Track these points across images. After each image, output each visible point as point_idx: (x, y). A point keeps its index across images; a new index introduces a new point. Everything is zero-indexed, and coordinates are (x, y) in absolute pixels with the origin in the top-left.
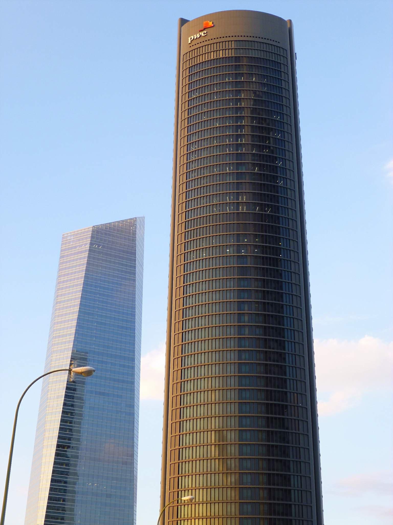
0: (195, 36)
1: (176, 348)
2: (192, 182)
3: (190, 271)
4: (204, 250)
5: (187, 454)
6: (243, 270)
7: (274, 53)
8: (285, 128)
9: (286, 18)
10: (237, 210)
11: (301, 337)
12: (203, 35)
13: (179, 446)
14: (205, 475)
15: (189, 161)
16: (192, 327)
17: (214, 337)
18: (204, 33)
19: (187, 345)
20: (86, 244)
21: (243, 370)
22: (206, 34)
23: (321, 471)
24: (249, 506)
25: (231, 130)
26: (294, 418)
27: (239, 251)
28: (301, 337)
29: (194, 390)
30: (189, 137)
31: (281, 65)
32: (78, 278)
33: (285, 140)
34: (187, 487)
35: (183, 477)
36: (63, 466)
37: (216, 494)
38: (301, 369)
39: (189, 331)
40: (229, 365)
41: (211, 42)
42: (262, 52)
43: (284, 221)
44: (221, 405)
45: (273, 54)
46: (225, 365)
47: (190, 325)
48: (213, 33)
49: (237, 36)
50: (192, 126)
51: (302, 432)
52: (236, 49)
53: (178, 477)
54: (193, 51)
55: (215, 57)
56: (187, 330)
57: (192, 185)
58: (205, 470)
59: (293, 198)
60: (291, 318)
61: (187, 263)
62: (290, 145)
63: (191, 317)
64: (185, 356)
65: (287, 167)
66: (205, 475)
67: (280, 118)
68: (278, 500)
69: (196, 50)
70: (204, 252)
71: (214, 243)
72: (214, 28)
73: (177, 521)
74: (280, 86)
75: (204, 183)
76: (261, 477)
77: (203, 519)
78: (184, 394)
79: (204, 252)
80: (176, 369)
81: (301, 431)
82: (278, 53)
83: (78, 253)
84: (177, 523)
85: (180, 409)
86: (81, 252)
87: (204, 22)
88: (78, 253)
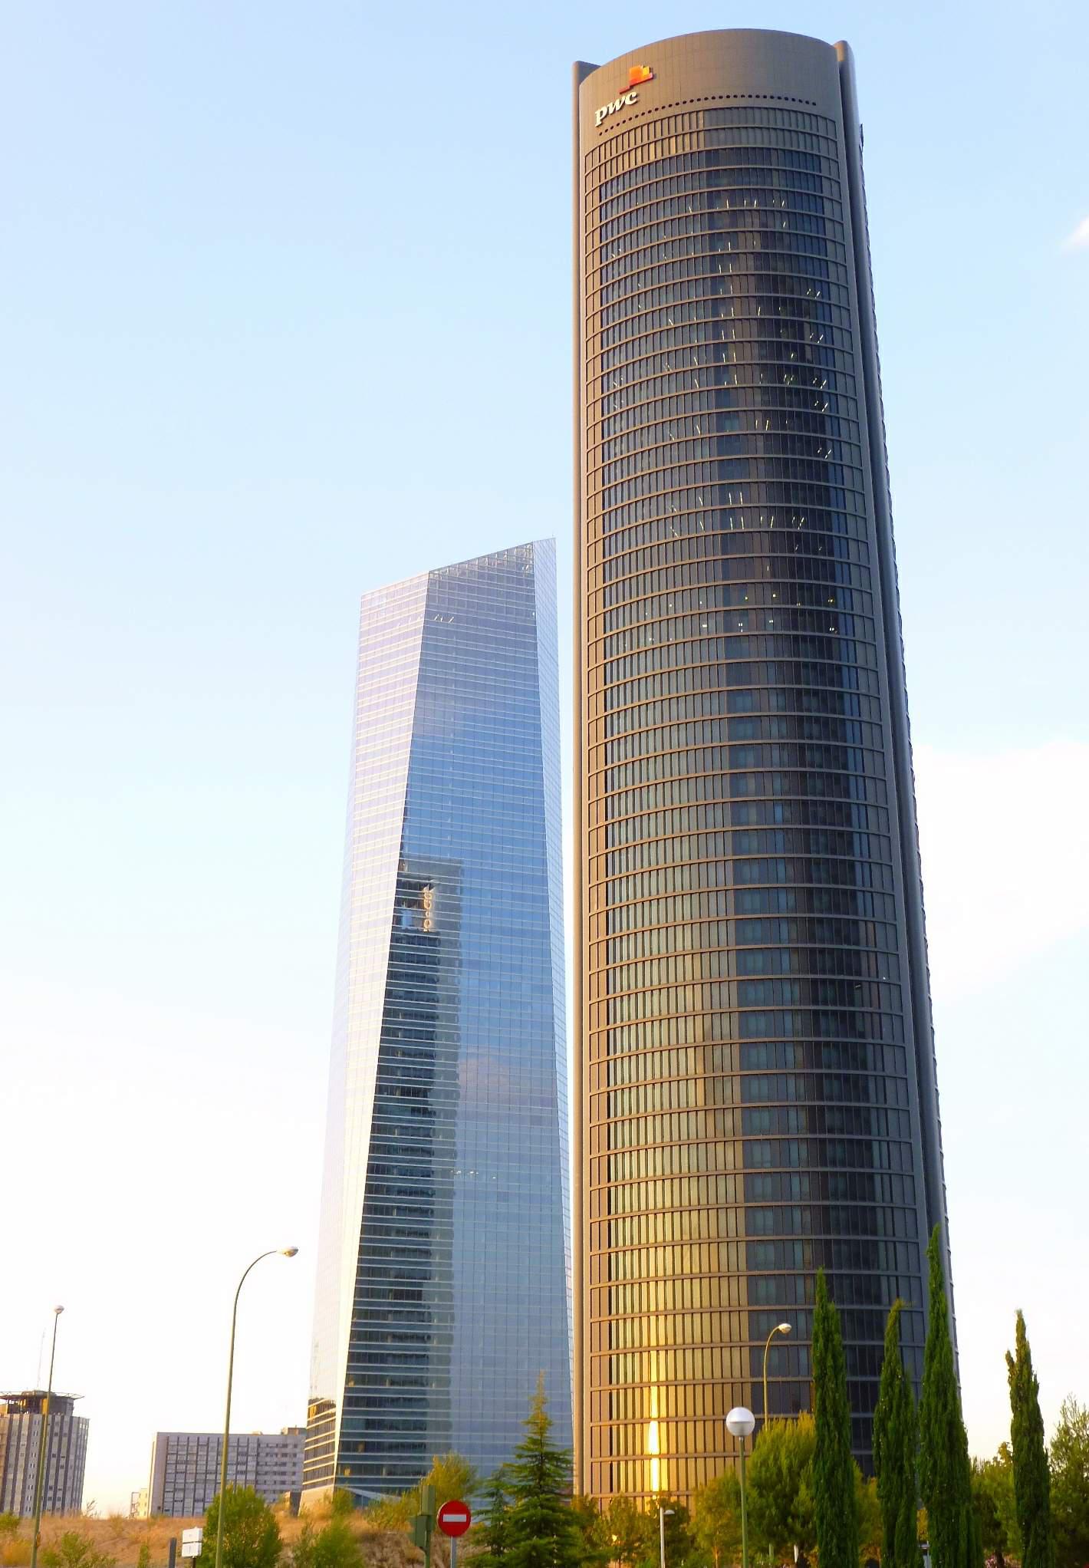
0: (610, 105)
1: (594, 862)
2: (615, 466)
3: (617, 628)
4: (649, 627)
5: (625, 1102)
6: (736, 671)
7: (801, 132)
8: (832, 296)
9: (831, 40)
10: (722, 528)
11: (883, 820)
12: (628, 102)
13: (608, 1085)
14: (667, 1150)
15: (607, 349)
16: (626, 785)
17: (675, 749)
18: (631, 98)
19: (616, 825)
20: (415, 617)
21: (747, 905)
22: (635, 101)
23: (960, 1357)
24: (772, 1284)
25: (702, 335)
26: (870, 1009)
27: (724, 525)
28: (883, 820)
29: (636, 957)
30: (606, 401)
31: (823, 183)
32: (402, 698)
33: (832, 302)
34: (627, 1176)
35: (620, 1156)
36: (394, 1134)
37: (692, 1192)
38: (862, 569)
39: (620, 850)
40: (711, 837)
41: (650, 118)
42: (773, 133)
43: (844, 649)
44: (695, 897)
45: (801, 136)
46: (702, 838)
47: (625, 808)
48: (653, 96)
49: (710, 98)
50: (613, 538)
51: (890, 1042)
52: (709, 130)
53: (609, 1156)
54: (608, 144)
55: (659, 157)
56: (617, 847)
57: (614, 337)
58: (667, 1138)
59: (843, 304)
60: (853, 696)
61: (611, 662)
62: (836, 206)
63: (623, 789)
64: (614, 968)
65: (842, 414)
66: (667, 1150)
67: (822, 296)
68: (834, 1163)
69: (614, 142)
70: (649, 633)
71: (671, 611)
72: (655, 81)
73: (610, 1355)
74: (820, 236)
75: (645, 466)
76: (783, 897)
77: (664, 1213)
78: (615, 998)
79: (649, 633)
80: (594, 910)
81: (887, 1040)
82: (814, 132)
83: (399, 637)
84: (610, 1359)
85: (607, 942)
86: (406, 635)
87: (631, 70)
88: (399, 637)
